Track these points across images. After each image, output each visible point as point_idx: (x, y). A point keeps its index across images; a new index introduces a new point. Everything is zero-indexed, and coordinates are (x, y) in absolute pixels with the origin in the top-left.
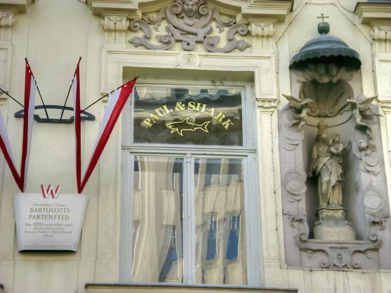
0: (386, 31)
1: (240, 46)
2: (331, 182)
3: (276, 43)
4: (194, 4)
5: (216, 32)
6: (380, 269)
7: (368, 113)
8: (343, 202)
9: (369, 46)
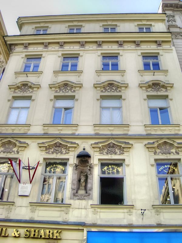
5: (63, 150)
7: (91, 167)
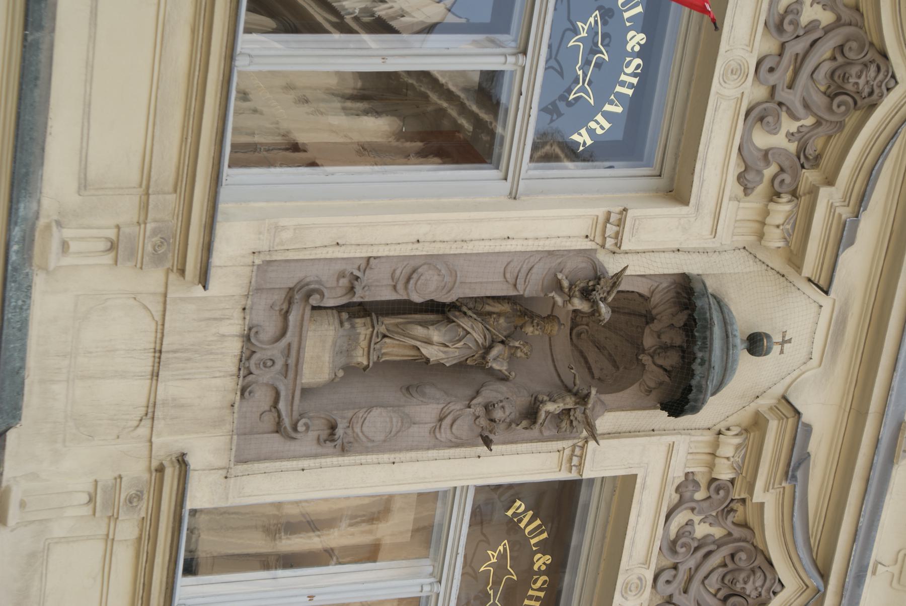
0: (732, 459)
1: (750, 176)
2: (430, 347)
3: (744, 248)
4: (858, 88)
5: (788, 125)
6: (238, 435)
7: (565, 424)
8: (386, 362)
9: (707, 425)
